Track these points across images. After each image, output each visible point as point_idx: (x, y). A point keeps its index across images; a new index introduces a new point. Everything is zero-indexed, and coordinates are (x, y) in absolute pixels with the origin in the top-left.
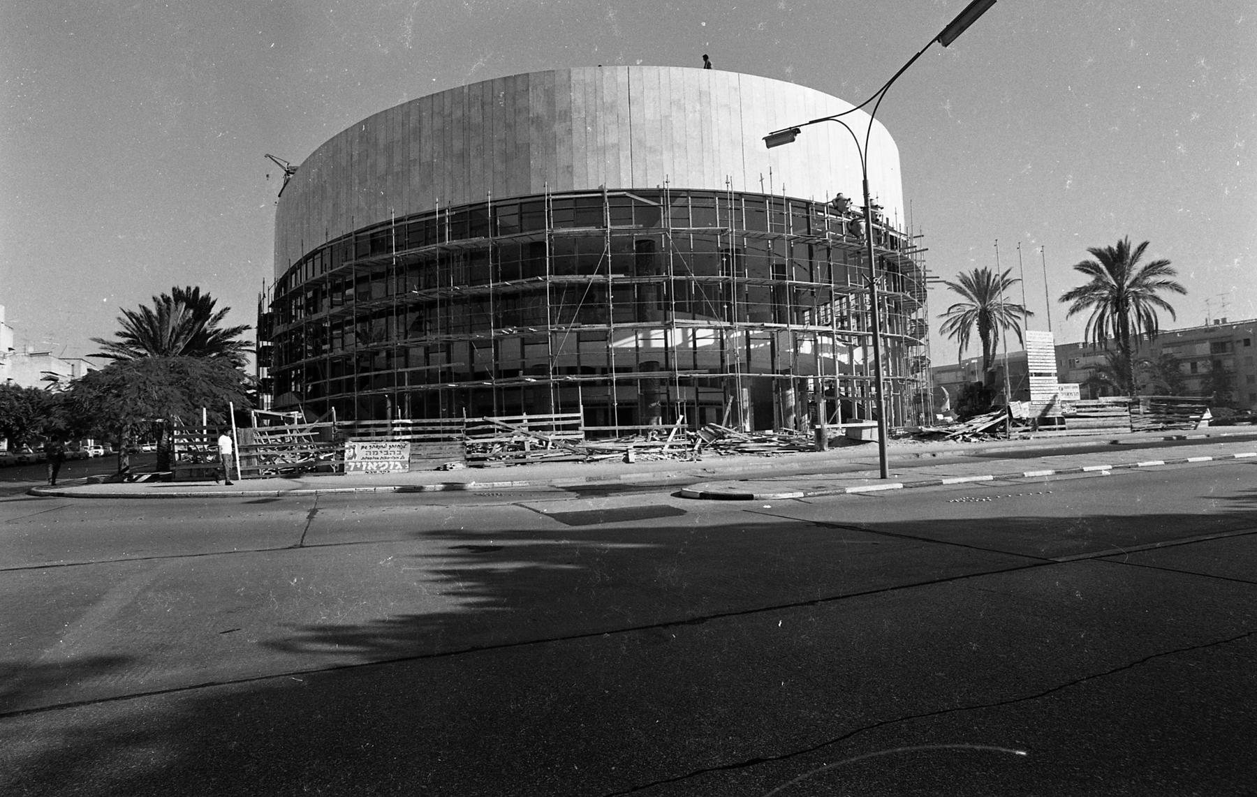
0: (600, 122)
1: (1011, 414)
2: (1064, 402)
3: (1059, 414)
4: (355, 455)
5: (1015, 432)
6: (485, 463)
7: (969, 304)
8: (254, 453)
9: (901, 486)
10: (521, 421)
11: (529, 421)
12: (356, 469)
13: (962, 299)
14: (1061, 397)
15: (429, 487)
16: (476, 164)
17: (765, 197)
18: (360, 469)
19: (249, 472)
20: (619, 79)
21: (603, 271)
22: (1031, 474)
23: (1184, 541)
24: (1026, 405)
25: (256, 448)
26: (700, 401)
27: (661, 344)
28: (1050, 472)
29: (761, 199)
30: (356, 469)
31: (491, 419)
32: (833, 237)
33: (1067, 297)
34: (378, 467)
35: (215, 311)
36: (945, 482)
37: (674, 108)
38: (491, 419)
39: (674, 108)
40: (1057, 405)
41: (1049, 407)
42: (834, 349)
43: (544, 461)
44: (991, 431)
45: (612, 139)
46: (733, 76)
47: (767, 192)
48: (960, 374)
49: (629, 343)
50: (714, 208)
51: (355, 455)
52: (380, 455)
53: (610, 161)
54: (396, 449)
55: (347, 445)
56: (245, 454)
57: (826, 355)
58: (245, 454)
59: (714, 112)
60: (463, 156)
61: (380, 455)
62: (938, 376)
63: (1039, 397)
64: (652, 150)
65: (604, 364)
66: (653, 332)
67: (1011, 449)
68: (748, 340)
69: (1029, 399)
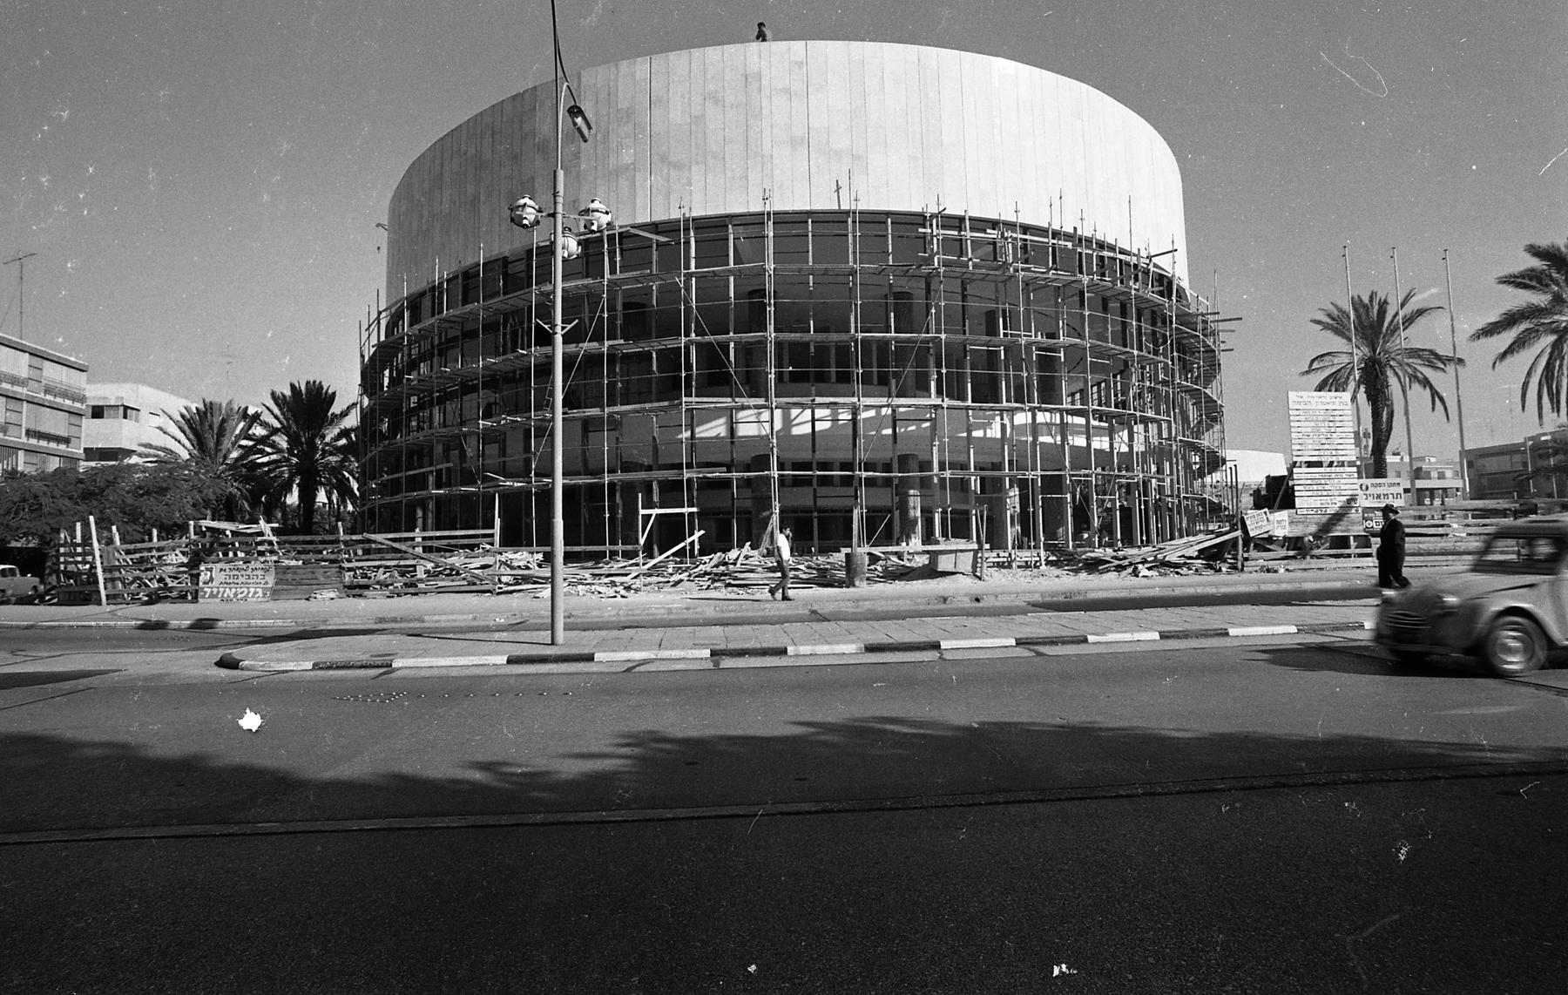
0: (613, 137)
1: (1245, 531)
2: (1366, 510)
3: (1359, 530)
4: (212, 579)
5: (1259, 559)
6: (366, 593)
7: (1349, 352)
8: (117, 574)
9: (1294, 629)
10: (413, 539)
11: (424, 538)
12: (212, 596)
13: (1338, 343)
14: (1363, 502)
15: (174, 623)
16: (484, 210)
17: (847, 213)
18: (216, 596)
19: (115, 596)
20: (638, 75)
21: (597, 337)
22: (805, 649)
23: (504, 820)
24: (1284, 515)
25: (118, 568)
26: (827, 512)
27: (807, 429)
28: (851, 648)
29: (803, 218)
30: (212, 596)
31: (373, 537)
32: (946, 264)
33: (1490, 330)
34: (236, 595)
35: (336, 408)
36: (1232, 632)
37: (709, 103)
38: (373, 537)
39: (709, 103)
40: (1355, 515)
41: (1337, 517)
42: (1088, 432)
43: (441, 591)
44: (1211, 556)
45: (627, 156)
46: (798, 46)
47: (845, 207)
48: (1517, 458)
49: (715, 429)
50: (886, 236)
51: (212, 579)
52: (241, 580)
53: (624, 184)
54: (259, 573)
55: (202, 568)
56: (109, 576)
57: (1048, 439)
58: (109, 576)
59: (765, 103)
60: (475, 201)
61: (241, 580)
62: (1480, 462)
63: (1315, 503)
64: (678, 166)
65: (845, 455)
66: (742, 415)
67: (1242, 589)
68: (813, 420)
69: (1292, 505)
